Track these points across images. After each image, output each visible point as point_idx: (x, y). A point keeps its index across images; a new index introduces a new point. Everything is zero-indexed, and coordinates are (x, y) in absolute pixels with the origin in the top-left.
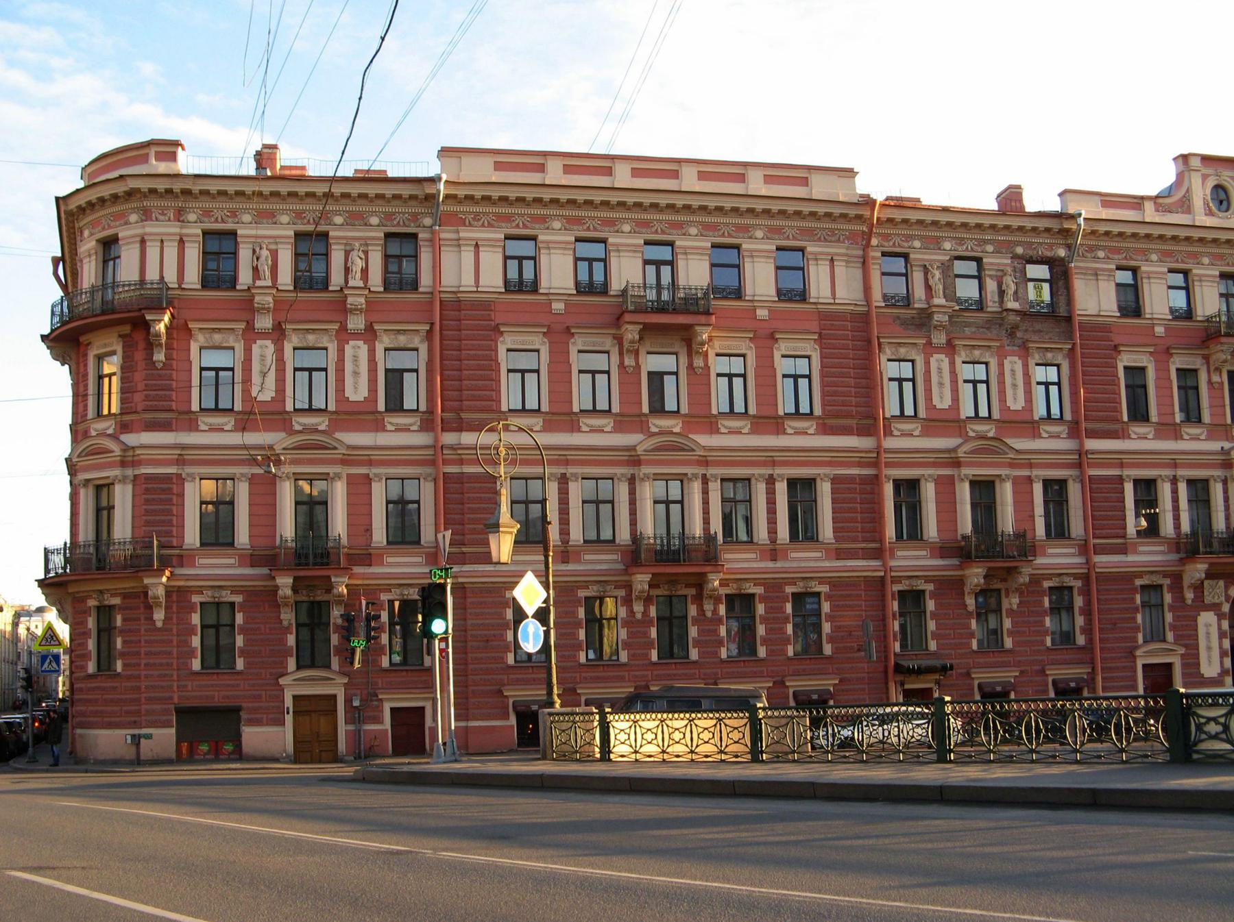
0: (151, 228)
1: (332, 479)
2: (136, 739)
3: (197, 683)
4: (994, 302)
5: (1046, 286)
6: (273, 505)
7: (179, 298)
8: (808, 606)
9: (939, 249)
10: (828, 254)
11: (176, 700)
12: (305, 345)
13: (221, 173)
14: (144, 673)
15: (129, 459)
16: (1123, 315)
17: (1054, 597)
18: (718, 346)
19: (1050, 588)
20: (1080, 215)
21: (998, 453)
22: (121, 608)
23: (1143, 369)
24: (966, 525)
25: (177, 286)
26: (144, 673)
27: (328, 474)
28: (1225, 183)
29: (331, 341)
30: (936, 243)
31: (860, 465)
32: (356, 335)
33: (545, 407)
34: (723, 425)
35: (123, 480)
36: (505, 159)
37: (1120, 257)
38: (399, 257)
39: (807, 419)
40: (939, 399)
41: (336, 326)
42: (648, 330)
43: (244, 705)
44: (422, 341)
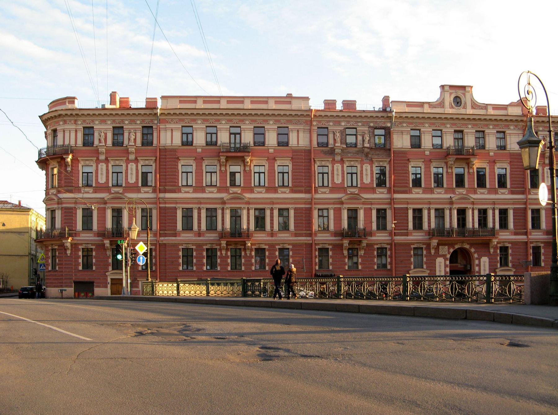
0: (66, 126)
1: (243, 209)
2: (62, 291)
3: (230, 274)
4: (361, 144)
5: (383, 138)
6: (105, 217)
7: (75, 150)
8: (285, 253)
9: (340, 125)
10: (296, 129)
11: (74, 279)
12: (115, 165)
13: (87, 108)
14: (64, 270)
15: (60, 201)
16: (412, 148)
17: (380, 251)
18: (255, 163)
19: (414, 248)
20: (393, 111)
21: (359, 199)
22: (58, 250)
23: (385, 167)
24: (345, 224)
25: (75, 146)
26: (64, 270)
27: (122, 207)
28: (459, 95)
29: (124, 163)
30: (339, 123)
31: (305, 204)
32: (132, 161)
33: (194, 185)
34: (256, 190)
35: (58, 209)
36: (183, 99)
37: (412, 126)
38: (147, 134)
39: (327, 188)
40: (337, 180)
41: (125, 158)
42: (228, 159)
43: (95, 281)
44: (153, 163)
